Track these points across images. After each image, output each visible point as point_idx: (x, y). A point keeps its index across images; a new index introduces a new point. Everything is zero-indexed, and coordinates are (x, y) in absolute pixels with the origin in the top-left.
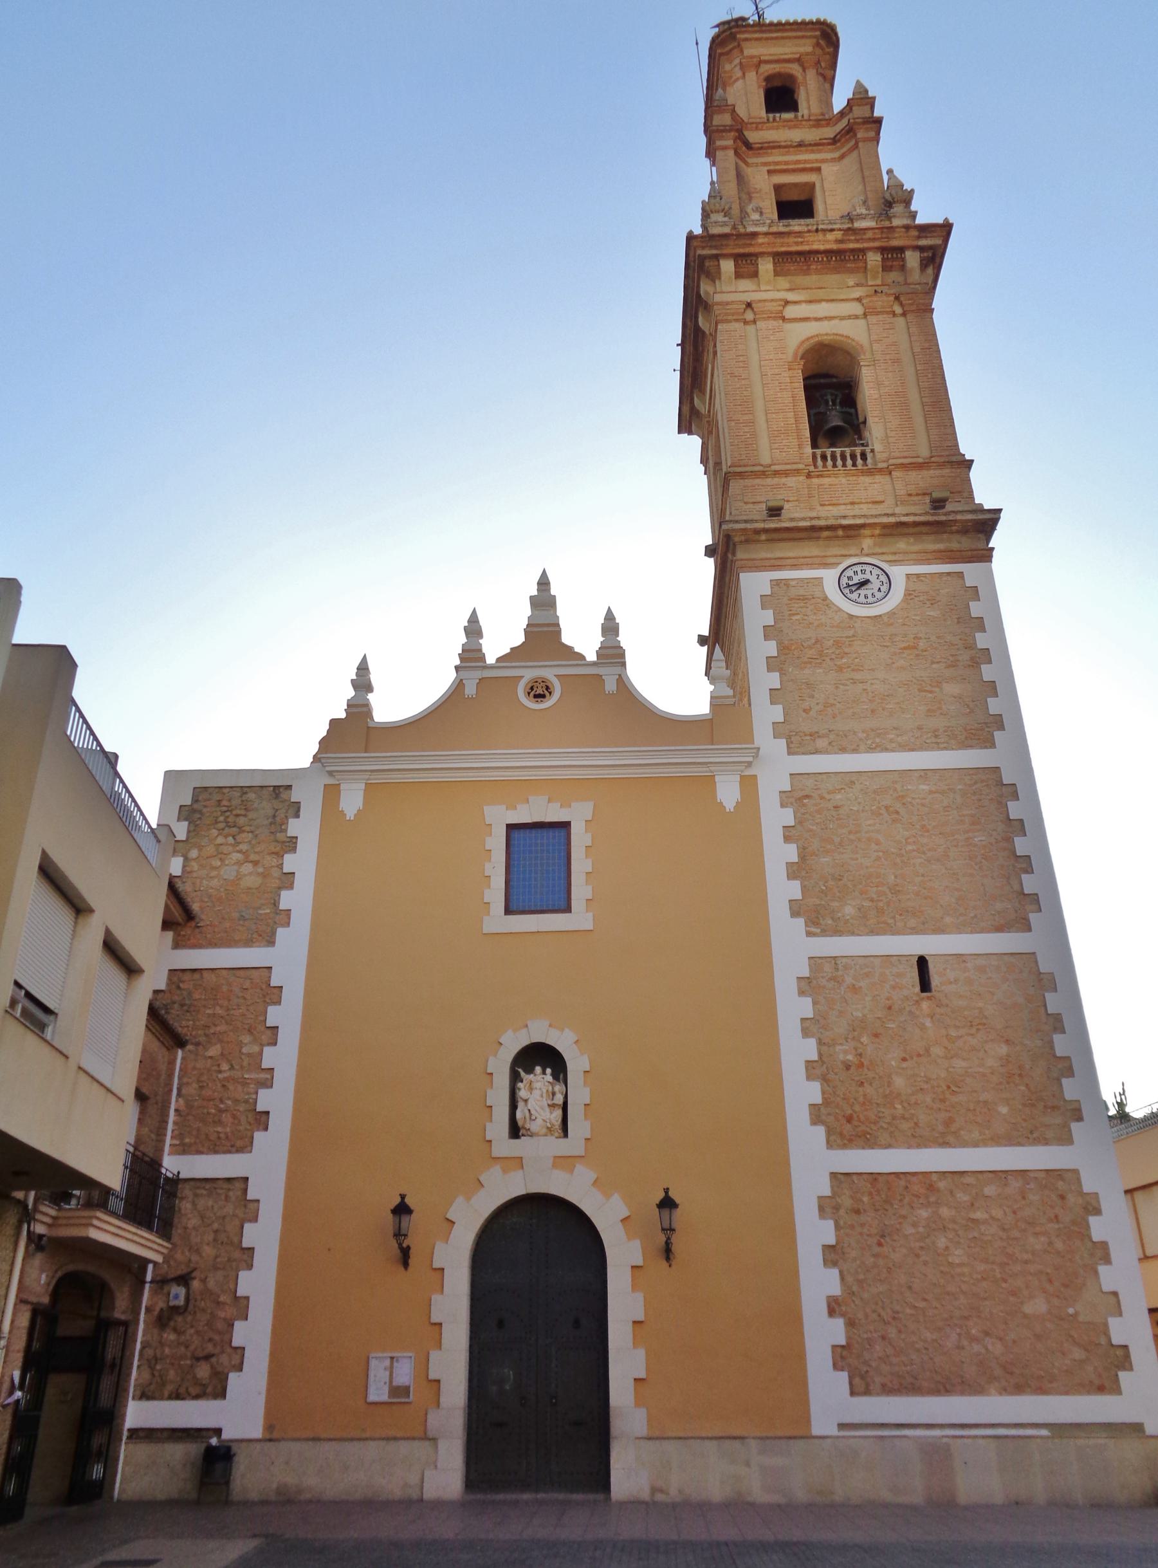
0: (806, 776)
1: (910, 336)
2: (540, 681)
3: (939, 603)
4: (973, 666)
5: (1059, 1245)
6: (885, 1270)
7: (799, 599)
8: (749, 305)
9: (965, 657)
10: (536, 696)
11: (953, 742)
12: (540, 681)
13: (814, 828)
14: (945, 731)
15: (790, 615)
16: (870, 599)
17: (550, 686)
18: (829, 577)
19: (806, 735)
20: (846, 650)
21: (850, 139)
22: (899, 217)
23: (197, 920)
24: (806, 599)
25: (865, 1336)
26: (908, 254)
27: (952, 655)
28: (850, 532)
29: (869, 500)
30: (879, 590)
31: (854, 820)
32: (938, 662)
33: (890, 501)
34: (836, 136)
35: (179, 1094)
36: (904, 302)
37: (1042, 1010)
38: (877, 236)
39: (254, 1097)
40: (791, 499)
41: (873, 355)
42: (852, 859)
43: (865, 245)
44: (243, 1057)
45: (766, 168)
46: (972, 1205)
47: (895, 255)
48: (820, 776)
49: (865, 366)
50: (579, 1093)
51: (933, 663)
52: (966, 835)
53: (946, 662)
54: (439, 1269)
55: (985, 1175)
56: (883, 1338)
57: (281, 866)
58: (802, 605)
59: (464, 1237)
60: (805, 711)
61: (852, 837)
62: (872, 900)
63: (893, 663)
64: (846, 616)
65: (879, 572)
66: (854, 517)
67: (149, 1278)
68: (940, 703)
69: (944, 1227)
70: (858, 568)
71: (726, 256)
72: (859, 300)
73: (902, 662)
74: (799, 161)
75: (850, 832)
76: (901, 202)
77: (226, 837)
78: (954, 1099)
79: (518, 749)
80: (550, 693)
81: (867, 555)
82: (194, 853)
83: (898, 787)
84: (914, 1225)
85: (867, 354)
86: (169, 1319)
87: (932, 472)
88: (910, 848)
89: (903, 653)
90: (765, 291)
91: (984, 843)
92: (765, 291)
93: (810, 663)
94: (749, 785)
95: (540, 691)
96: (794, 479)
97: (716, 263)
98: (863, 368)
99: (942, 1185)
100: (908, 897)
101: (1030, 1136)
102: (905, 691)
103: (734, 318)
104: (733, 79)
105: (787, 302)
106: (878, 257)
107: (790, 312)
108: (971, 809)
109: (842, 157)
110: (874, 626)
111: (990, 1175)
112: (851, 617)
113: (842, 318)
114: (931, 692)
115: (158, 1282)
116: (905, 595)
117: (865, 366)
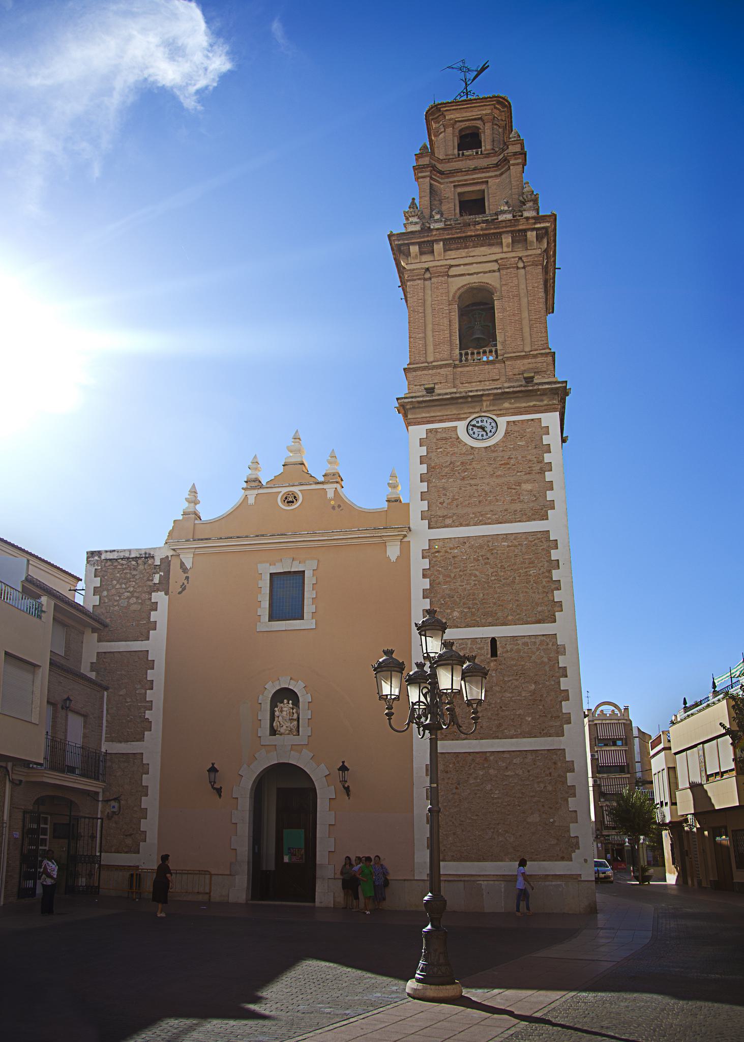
0: (438, 540)
1: (526, 280)
2: (291, 493)
3: (525, 437)
4: (541, 473)
5: (550, 788)
6: (458, 801)
7: (442, 439)
8: (427, 269)
9: (537, 468)
10: (288, 502)
11: (524, 517)
12: (291, 493)
13: (440, 569)
14: (520, 511)
15: (436, 449)
16: (485, 437)
17: (297, 496)
18: (461, 426)
19: (440, 517)
20: (468, 467)
21: (506, 164)
22: (527, 210)
23: (110, 627)
24: (447, 439)
25: (445, 833)
26: (529, 233)
27: (529, 467)
28: (477, 399)
29: (490, 379)
30: (491, 431)
31: (464, 564)
32: (521, 472)
33: (503, 379)
34: (497, 163)
35: (108, 713)
36: (524, 261)
37: (557, 664)
38: (507, 225)
39: (144, 714)
40: (442, 381)
41: (501, 293)
42: (460, 586)
43: (501, 230)
44: (137, 695)
45: (453, 184)
46: (507, 768)
47: (520, 234)
48: (446, 540)
49: (496, 300)
50: (305, 714)
51: (518, 472)
52: (526, 570)
53: (525, 471)
54: (236, 798)
55: (515, 753)
56: (454, 834)
57: (150, 599)
58: (444, 442)
59: (248, 782)
60: (440, 503)
61: (461, 573)
62: (469, 608)
63: (494, 473)
64: (469, 448)
65: (491, 421)
66: (477, 391)
67: (101, 799)
68: (519, 495)
69: (491, 779)
70: (479, 419)
71: (413, 244)
72: (496, 261)
73: (499, 473)
74: (474, 178)
75: (460, 571)
76: (530, 201)
77: (121, 584)
78: (503, 714)
79: (63, 608)
80: (296, 500)
81: (484, 412)
82: (105, 593)
83: (490, 544)
84: (475, 778)
85: (498, 293)
86: (112, 817)
87: (530, 360)
88: (493, 578)
89: (500, 467)
90: (438, 260)
91: (535, 574)
92: (438, 260)
93: (446, 476)
94: (405, 548)
95: (290, 499)
96: (445, 369)
97: (408, 248)
98: (495, 301)
99: (492, 758)
100: (489, 605)
101: (542, 732)
102: (499, 489)
103: (418, 277)
104: (440, 132)
105: (451, 266)
106: (417, 247)
107: (453, 271)
108: (530, 555)
109: (501, 174)
110: (486, 452)
111: (518, 753)
112: (472, 448)
113: (485, 273)
114: (514, 489)
115: (105, 801)
116: (505, 434)
117: (496, 300)
